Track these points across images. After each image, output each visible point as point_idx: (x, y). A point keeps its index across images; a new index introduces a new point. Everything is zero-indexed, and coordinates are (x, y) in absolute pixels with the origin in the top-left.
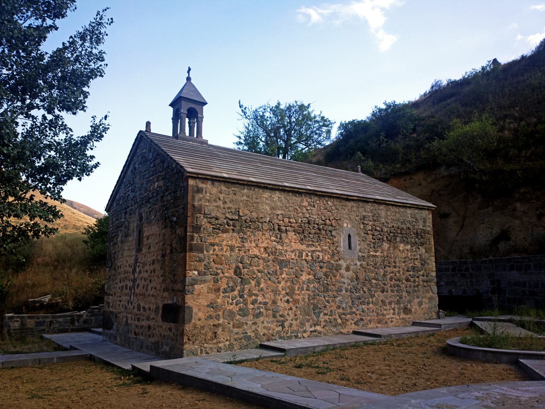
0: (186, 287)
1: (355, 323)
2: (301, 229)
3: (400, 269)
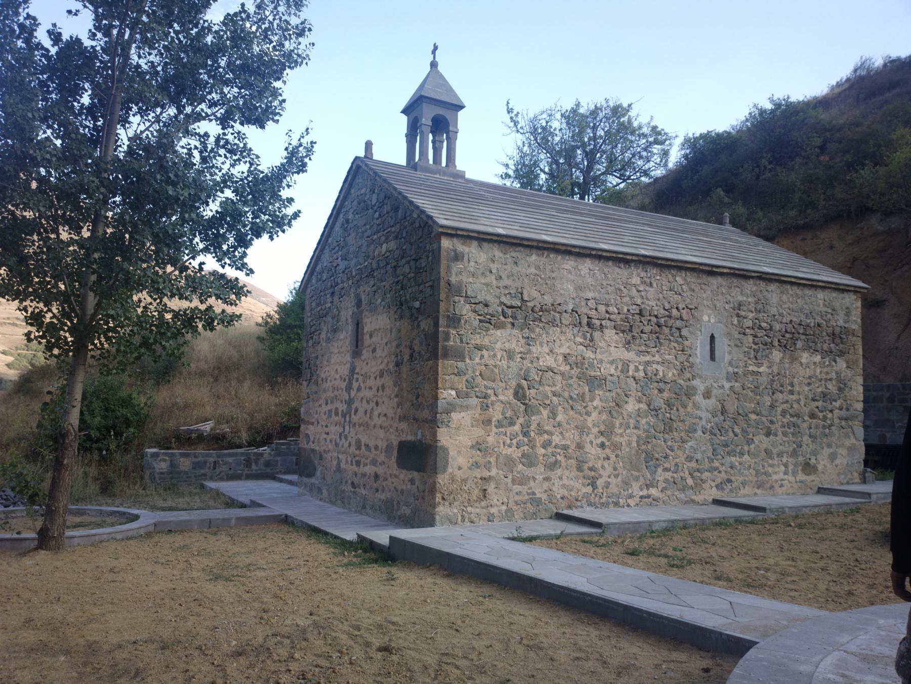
0: (438, 415)
1: (717, 486)
2: (628, 324)
3: (801, 397)
